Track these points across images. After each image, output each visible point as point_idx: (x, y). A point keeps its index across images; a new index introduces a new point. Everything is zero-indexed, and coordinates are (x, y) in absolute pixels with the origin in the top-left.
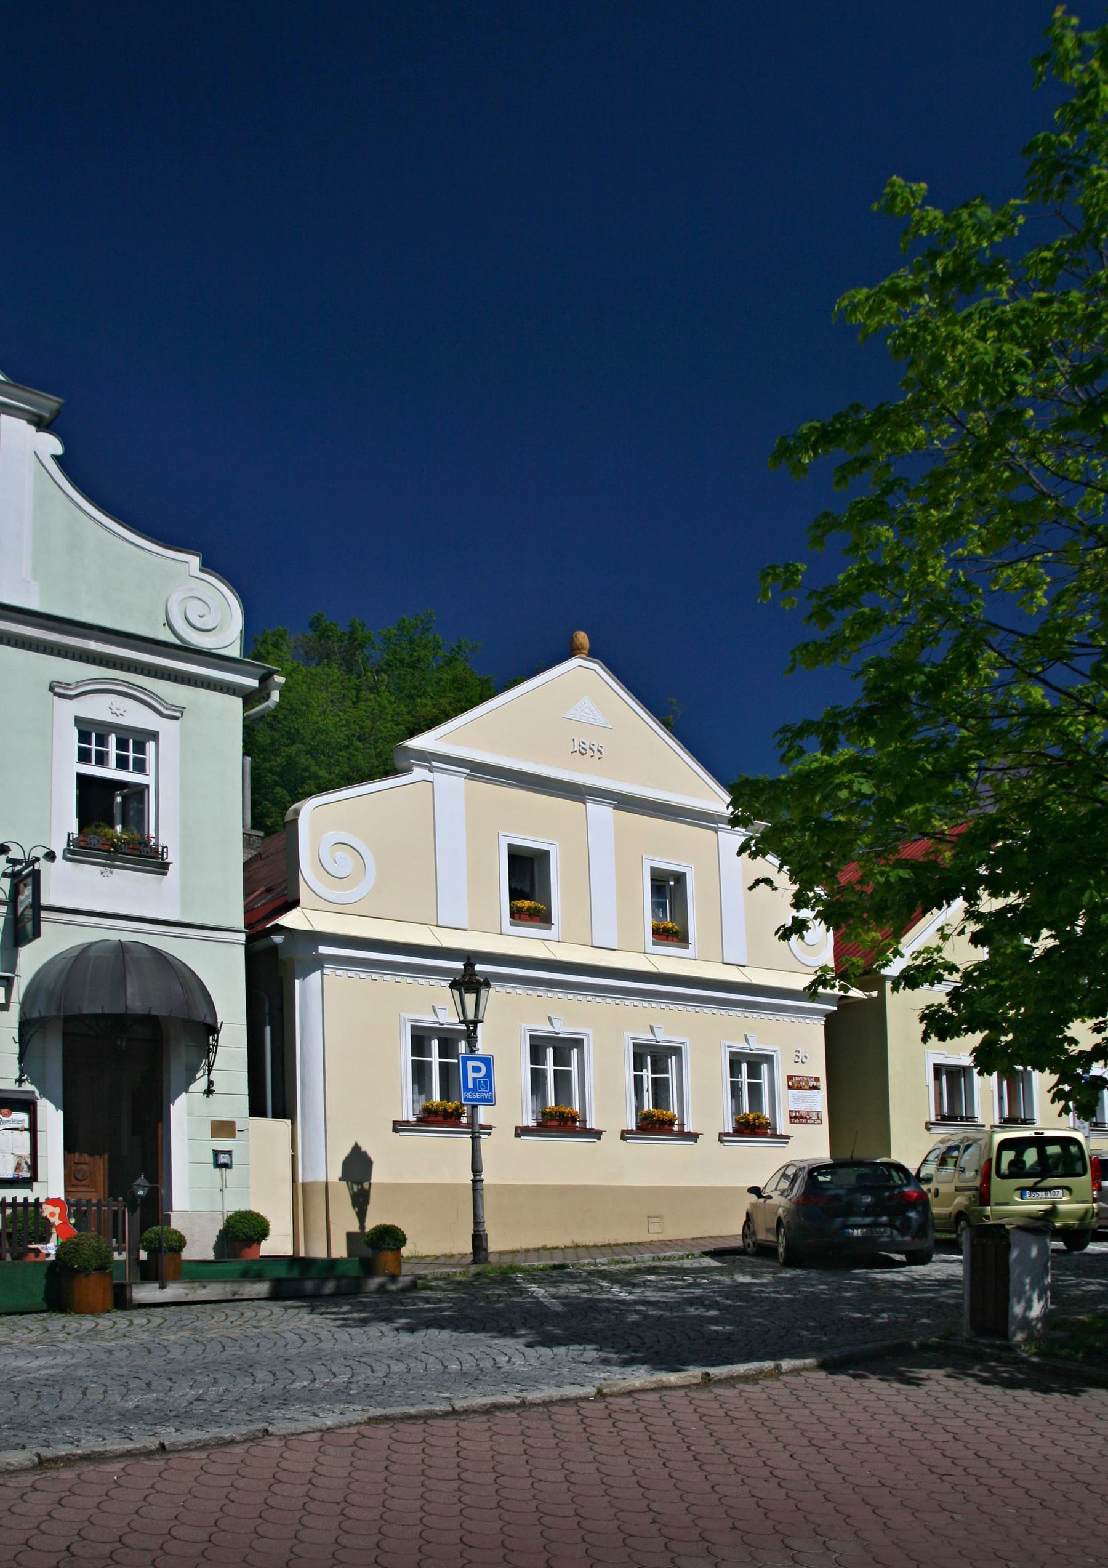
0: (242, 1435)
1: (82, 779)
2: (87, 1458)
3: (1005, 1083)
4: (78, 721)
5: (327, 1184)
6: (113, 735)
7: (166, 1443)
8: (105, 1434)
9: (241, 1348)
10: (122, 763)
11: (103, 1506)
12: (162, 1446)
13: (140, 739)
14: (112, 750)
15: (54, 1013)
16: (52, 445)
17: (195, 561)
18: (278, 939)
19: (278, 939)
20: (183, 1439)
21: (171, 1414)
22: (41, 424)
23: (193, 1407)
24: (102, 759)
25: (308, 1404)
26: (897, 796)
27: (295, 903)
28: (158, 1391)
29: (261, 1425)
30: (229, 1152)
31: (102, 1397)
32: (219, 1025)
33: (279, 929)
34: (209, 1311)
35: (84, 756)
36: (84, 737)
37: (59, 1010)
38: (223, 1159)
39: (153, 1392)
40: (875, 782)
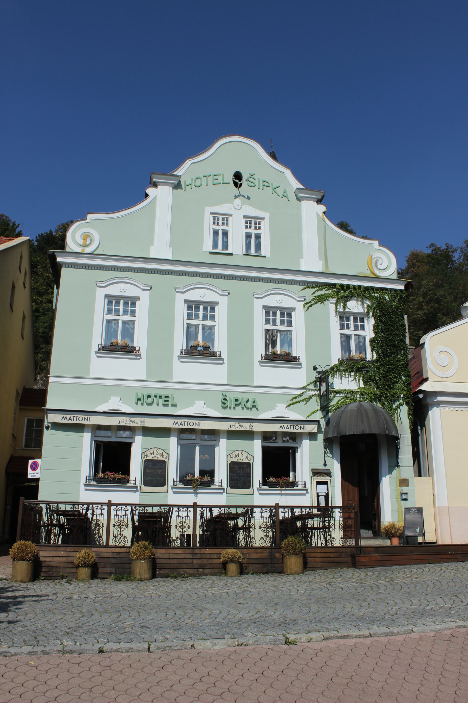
0: (402, 632)
1: (267, 331)
2: (342, 637)
3: (179, 447)
4: (264, 307)
5: (448, 507)
6: (352, 316)
7: (372, 633)
8: (350, 627)
9: (409, 588)
10: (282, 323)
11: (364, 659)
12: (370, 634)
13: (362, 316)
14: (278, 318)
15: (335, 435)
16: (322, 208)
17: (376, 243)
18: (421, 396)
19: (421, 396)
20: (380, 632)
21: (376, 619)
22: (319, 201)
23: (386, 616)
24: (274, 322)
25: (432, 617)
26: (453, 261)
27: (427, 379)
28: (372, 608)
29: (410, 627)
30: (406, 493)
31: (350, 610)
32: (399, 435)
33: (421, 391)
34: (398, 570)
35: (268, 322)
36: (267, 313)
37: (337, 434)
38: (404, 497)
39: (371, 608)
40: (457, 257)
